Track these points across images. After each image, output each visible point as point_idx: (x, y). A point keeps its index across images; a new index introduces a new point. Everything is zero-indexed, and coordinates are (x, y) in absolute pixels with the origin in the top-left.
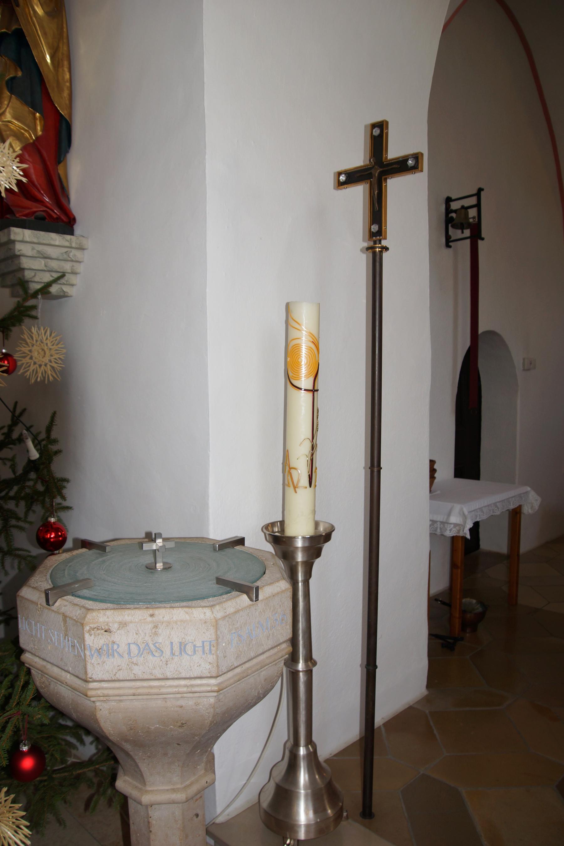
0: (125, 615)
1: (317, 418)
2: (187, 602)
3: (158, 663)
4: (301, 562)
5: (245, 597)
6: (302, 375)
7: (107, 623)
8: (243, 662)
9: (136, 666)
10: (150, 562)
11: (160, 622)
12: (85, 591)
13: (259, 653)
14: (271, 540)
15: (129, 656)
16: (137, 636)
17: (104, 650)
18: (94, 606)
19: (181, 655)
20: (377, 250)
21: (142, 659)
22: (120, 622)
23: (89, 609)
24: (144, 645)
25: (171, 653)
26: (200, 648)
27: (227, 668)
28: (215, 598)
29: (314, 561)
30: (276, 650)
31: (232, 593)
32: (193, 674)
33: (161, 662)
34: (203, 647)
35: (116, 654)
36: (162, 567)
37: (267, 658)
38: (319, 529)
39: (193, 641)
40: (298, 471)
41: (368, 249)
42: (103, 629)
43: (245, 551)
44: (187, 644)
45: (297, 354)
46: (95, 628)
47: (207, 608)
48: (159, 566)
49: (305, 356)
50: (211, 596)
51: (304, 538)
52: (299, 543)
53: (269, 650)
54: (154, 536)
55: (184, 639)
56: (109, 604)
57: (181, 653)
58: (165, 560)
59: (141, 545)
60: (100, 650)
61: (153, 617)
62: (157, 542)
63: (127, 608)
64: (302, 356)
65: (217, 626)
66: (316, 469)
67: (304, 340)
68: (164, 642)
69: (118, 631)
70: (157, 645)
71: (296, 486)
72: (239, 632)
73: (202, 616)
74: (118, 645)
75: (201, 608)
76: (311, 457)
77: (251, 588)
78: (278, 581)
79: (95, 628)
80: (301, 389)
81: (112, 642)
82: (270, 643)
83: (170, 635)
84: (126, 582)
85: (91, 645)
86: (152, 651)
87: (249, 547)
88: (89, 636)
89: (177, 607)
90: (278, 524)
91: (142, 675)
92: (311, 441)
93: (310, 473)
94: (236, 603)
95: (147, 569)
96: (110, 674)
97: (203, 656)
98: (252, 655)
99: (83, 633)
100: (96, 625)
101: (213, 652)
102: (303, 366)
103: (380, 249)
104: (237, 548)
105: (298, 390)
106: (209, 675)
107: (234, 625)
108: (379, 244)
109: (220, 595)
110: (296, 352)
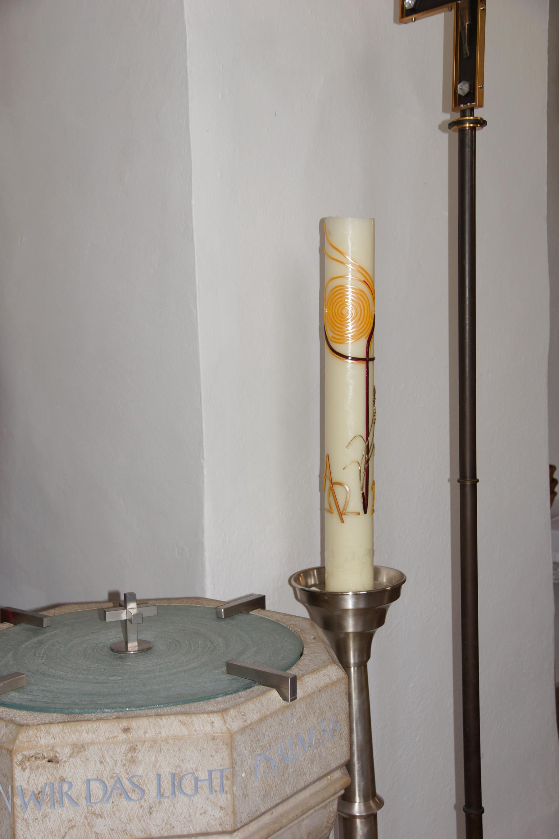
0: (82, 731)
1: (374, 402)
2: (183, 706)
3: (136, 811)
4: (353, 633)
5: (274, 694)
6: (348, 335)
7: (53, 747)
8: (275, 804)
9: (100, 818)
10: (115, 640)
11: (140, 741)
12: (13, 694)
13: (299, 787)
14: (304, 598)
15: (89, 802)
16: (103, 767)
17: (47, 795)
18: (29, 719)
19: (174, 796)
20: (467, 125)
21: (110, 805)
22: (74, 745)
23: (21, 725)
24: (113, 781)
25: (157, 793)
26: (206, 782)
27: (249, 815)
28: (228, 696)
29: (375, 632)
30: (324, 782)
31: (253, 688)
32: (193, 828)
33: (142, 809)
34: (211, 780)
35: (66, 800)
36: (136, 649)
37: (311, 795)
38: (380, 579)
39: (194, 770)
40: (345, 488)
41: (452, 125)
42: (46, 758)
43: (268, 618)
44: (184, 776)
45: (339, 302)
46: (32, 756)
47: (215, 715)
48: (133, 646)
49: (352, 304)
50: (220, 694)
51: (357, 595)
52: (350, 603)
53: (314, 782)
54: (122, 598)
55: (179, 768)
56: (55, 714)
57: (174, 793)
58: (141, 637)
59: (102, 615)
60: (39, 794)
61: (129, 732)
62: (128, 608)
63: (85, 719)
64: (348, 304)
65: (233, 743)
66: (374, 483)
67: (350, 279)
68: (147, 775)
69: (71, 759)
70: (135, 780)
71: (343, 511)
72: (267, 752)
73: (208, 728)
74: (70, 784)
75: (205, 715)
76: (365, 465)
77: (283, 679)
78: (325, 667)
79: (32, 756)
80: (346, 357)
81: (60, 778)
82: (316, 771)
83: (157, 762)
84: (80, 676)
85: (25, 786)
86: (127, 791)
87: (273, 612)
88: (22, 771)
89: (167, 715)
90: (314, 573)
91: (110, 834)
92: (365, 439)
93: (364, 491)
94: (262, 704)
95: (112, 652)
96: (55, 836)
97: (211, 797)
98: (288, 791)
99: (12, 767)
100: (34, 752)
101: (226, 789)
102: (349, 321)
103: (472, 125)
104: (253, 613)
105: (342, 359)
106: (220, 829)
107: (259, 741)
108: (471, 116)
109: (235, 693)
110: (338, 299)
